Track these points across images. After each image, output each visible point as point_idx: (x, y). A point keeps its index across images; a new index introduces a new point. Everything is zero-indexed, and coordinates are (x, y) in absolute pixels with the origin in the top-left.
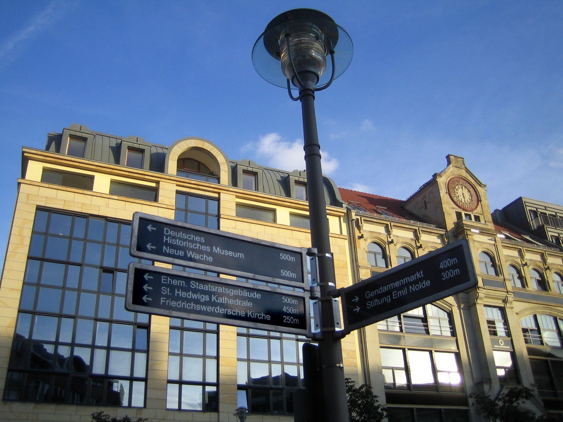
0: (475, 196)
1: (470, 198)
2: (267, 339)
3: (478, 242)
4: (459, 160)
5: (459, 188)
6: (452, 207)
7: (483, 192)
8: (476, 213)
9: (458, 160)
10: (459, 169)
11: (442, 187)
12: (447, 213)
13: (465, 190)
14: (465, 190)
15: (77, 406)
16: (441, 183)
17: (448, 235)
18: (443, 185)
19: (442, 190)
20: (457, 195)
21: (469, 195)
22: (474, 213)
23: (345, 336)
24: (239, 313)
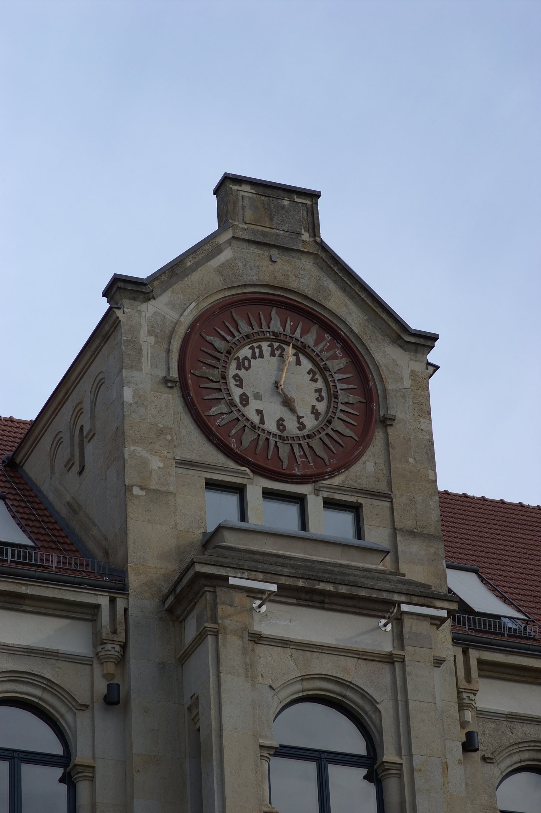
0: (352, 399)
1: (321, 407)
2: (12, 759)
3: (284, 643)
4: (286, 203)
5: (261, 356)
6: (188, 456)
7: (413, 373)
8: (340, 489)
9: (283, 207)
10: (274, 252)
11: (146, 352)
12: (143, 493)
13: (298, 363)
14: (298, 363)
15: (390, 507)
16: (143, 332)
17: (126, 610)
18: (152, 339)
19: (140, 370)
20: (236, 392)
21: (318, 391)
22: (331, 488)
23: (370, 782)
24: (6, 556)
